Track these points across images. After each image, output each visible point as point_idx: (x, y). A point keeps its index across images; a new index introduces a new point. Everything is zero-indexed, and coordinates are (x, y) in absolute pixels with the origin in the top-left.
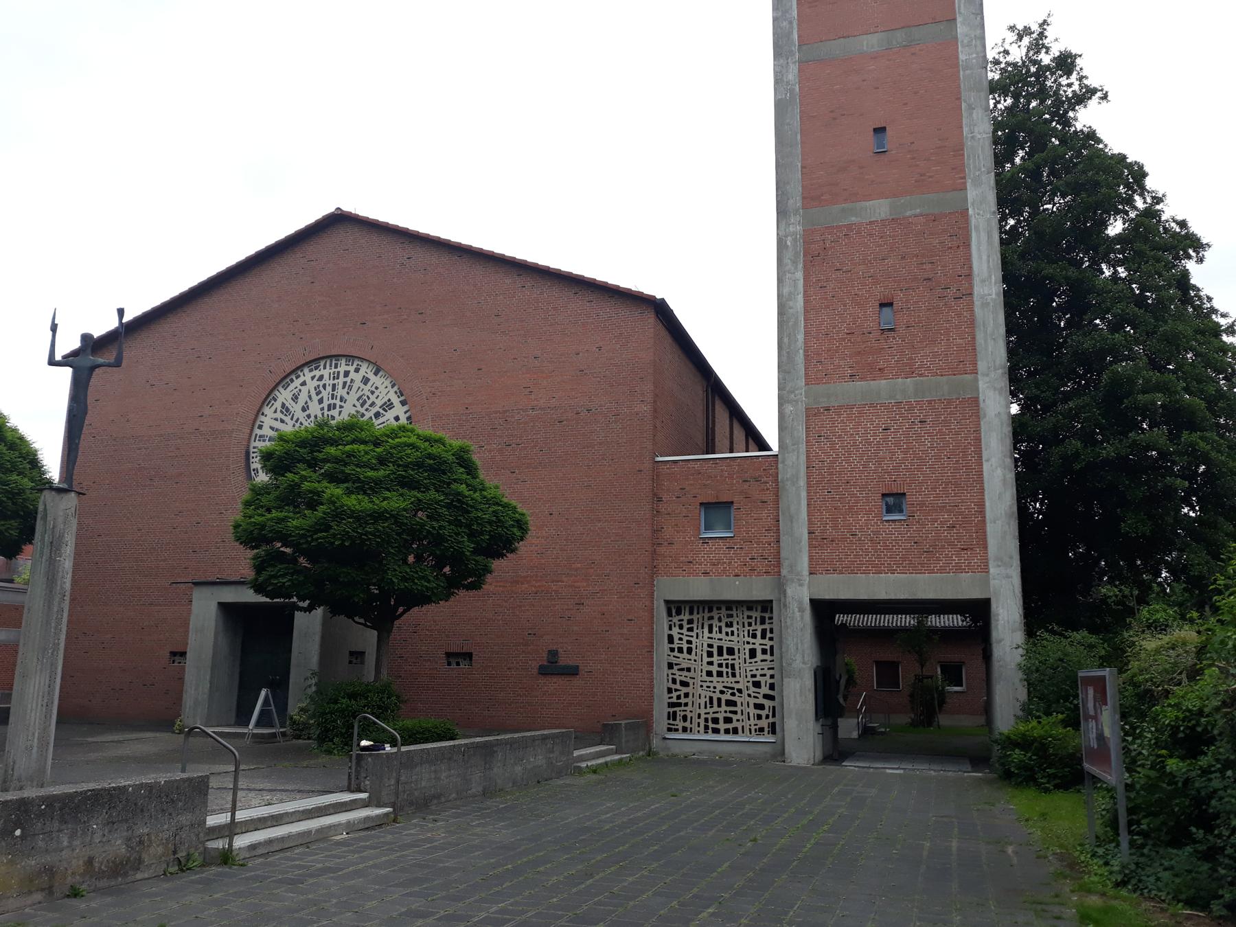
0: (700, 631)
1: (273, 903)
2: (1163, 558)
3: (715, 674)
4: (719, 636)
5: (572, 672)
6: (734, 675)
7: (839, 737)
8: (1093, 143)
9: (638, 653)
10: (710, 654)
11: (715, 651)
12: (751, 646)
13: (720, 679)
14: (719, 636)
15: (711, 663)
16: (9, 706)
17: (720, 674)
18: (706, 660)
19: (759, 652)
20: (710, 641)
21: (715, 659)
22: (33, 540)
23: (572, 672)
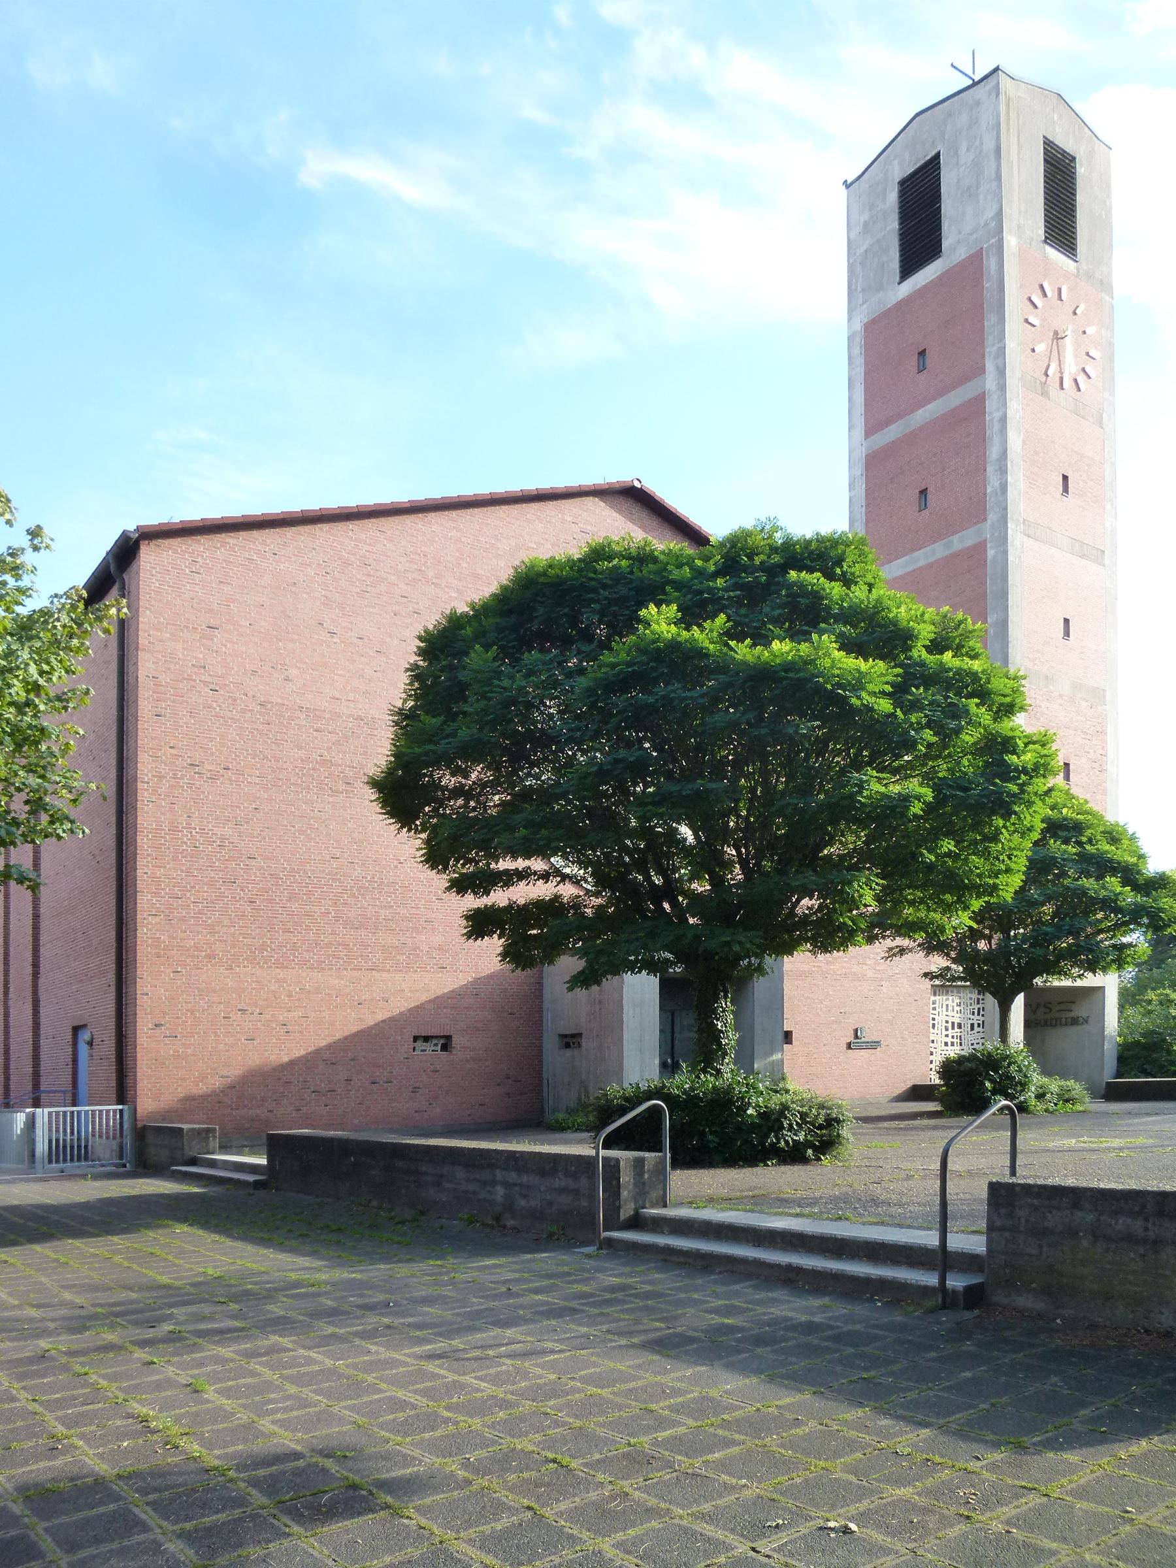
0: (940, 1010)
1: (816, 1342)
2: (1087, 936)
3: (949, 1044)
4: (952, 1014)
5: (874, 1045)
6: (961, 1045)
7: (628, 978)
8: (746, 961)
9: (233, 929)
10: (947, 1029)
11: (950, 1025)
12: (971, 1022)
13: (953, 1048)
14: (952, 1014)
15: (947, 1036)
16: (960, 541)
17: (953, 1044)
18: (945, 1033)
19: (976, 1025)
20: (947, 1018)
21: (950, 1032)
22: (475, 893)
23: (874, 1045)
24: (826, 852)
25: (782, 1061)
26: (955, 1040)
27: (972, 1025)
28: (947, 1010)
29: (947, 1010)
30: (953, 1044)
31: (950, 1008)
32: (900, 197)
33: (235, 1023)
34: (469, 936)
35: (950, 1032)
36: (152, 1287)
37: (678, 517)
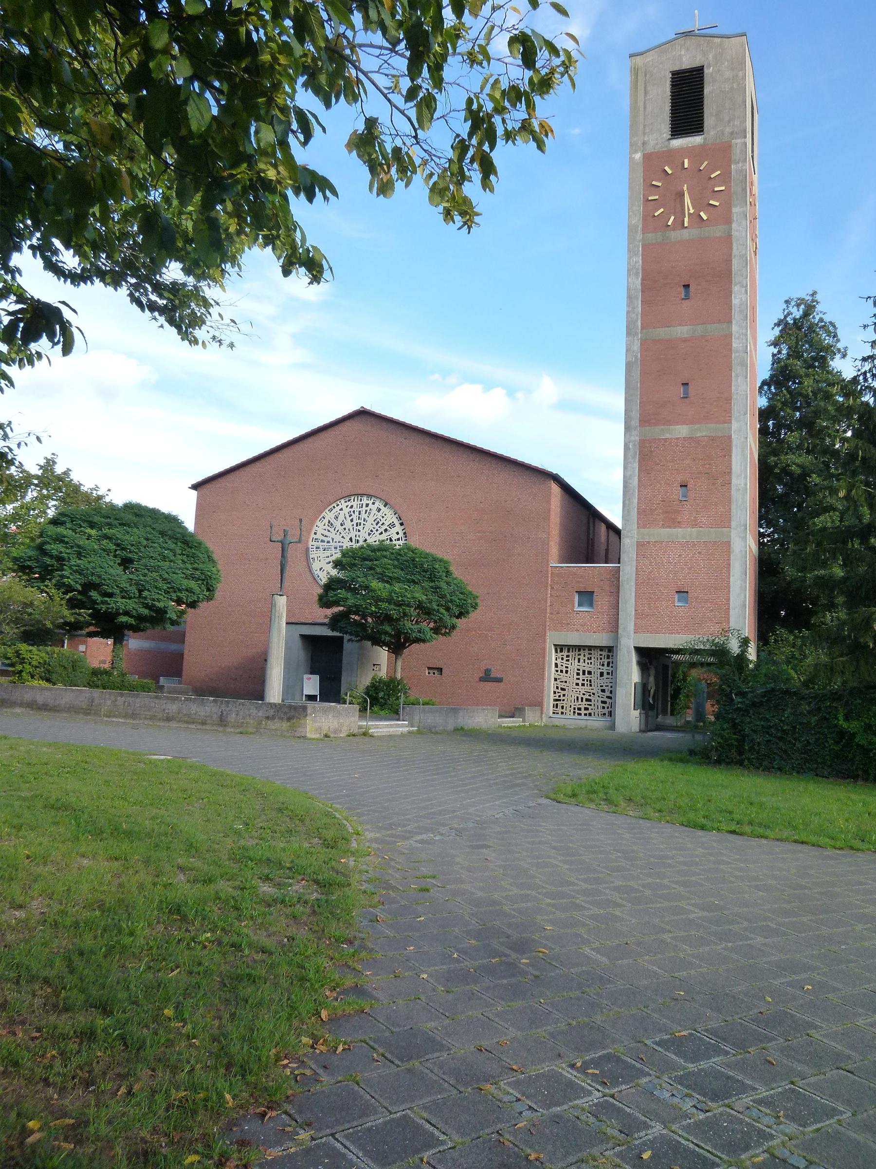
10: (578, 674)
11: (581, 672)
15: (578, 679)
17: (583, 685)
18: (576, 677)
21: (581, 676)
24: (240, 93)
25: (345, 703)
26: (585, 682)
27: (567, 672)
28: (579, 661)
29: (579, 661)
30: (583, 685)
31: (581, 661)
32: (703, 87)
33: (70, 1084)
34: (674, 73)
35: (581, 676)
36: (813, 845)
37: (759, 631)
